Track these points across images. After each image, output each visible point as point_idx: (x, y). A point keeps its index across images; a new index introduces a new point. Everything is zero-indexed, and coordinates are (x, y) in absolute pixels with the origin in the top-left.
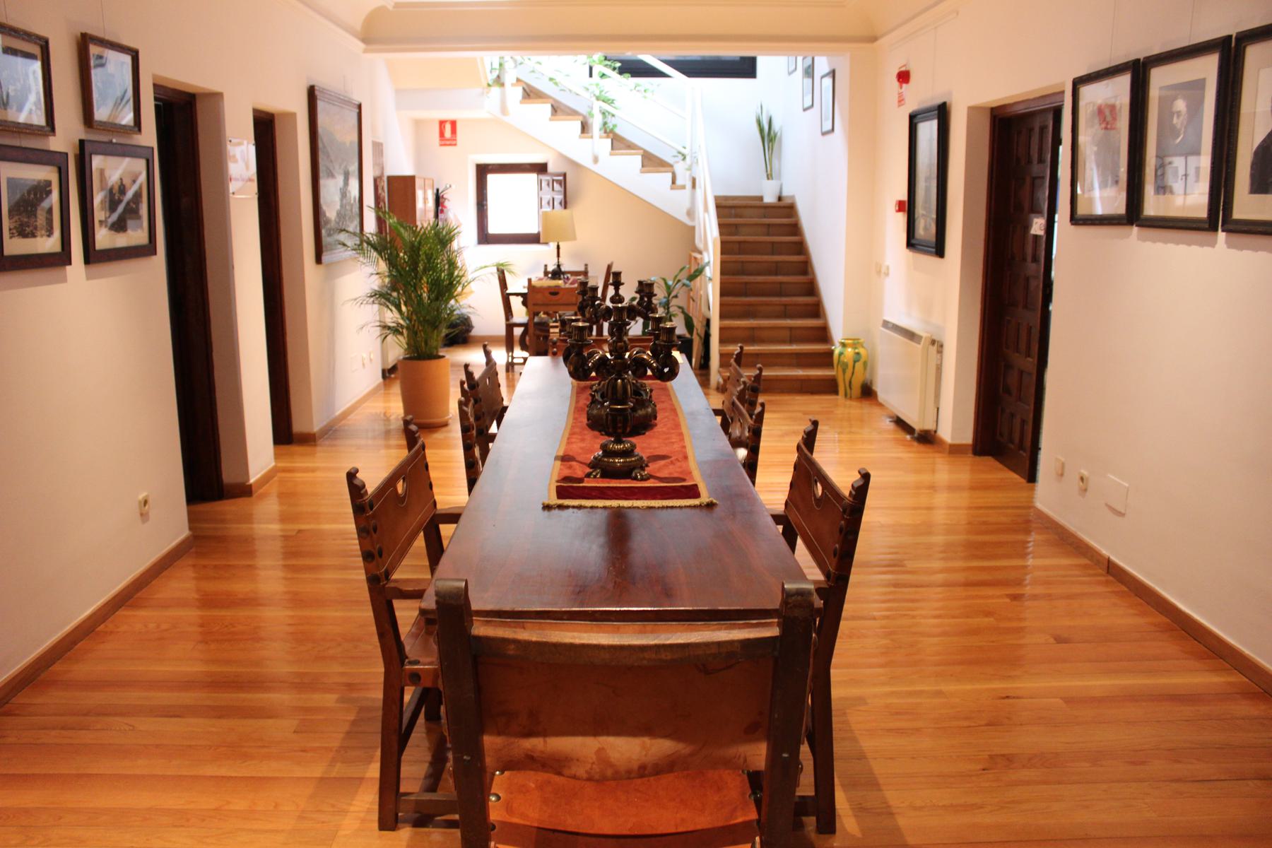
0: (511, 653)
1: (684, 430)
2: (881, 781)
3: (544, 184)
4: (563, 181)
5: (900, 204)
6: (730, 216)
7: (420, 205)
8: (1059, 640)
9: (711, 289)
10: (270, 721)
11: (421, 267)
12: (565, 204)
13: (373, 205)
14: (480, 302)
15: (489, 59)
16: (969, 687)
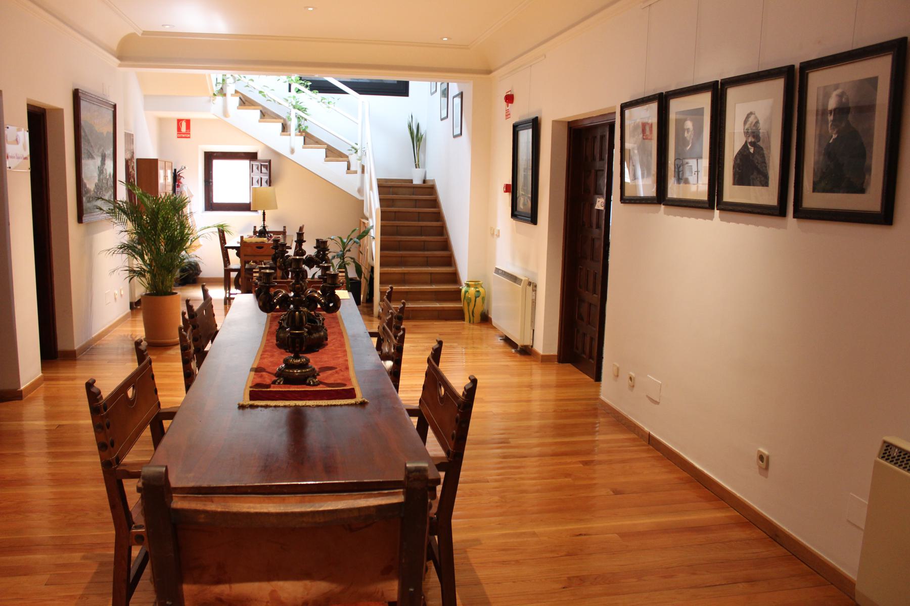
0: (202, 520)
1: (347, 348)
2: (491, 600)
3: (255, 168)
4: (268, 165)
5: (507, 186)
6: (389, 194)
7: (161, 180)
8: (616, 492)
9: (374, 246)
10: (24, 578)
11: (159, 226)
12: (270, 183)
13: (124, 180)
14: (205, 252)
15: (215, 76)
16: (554, 529)
